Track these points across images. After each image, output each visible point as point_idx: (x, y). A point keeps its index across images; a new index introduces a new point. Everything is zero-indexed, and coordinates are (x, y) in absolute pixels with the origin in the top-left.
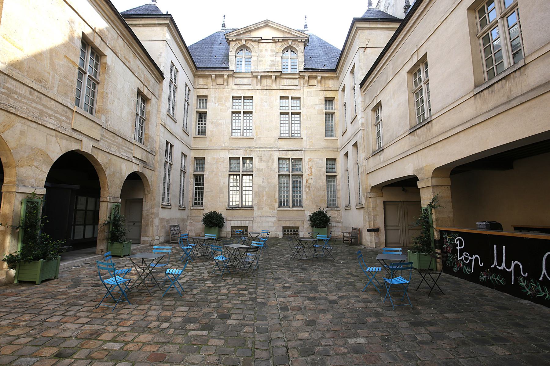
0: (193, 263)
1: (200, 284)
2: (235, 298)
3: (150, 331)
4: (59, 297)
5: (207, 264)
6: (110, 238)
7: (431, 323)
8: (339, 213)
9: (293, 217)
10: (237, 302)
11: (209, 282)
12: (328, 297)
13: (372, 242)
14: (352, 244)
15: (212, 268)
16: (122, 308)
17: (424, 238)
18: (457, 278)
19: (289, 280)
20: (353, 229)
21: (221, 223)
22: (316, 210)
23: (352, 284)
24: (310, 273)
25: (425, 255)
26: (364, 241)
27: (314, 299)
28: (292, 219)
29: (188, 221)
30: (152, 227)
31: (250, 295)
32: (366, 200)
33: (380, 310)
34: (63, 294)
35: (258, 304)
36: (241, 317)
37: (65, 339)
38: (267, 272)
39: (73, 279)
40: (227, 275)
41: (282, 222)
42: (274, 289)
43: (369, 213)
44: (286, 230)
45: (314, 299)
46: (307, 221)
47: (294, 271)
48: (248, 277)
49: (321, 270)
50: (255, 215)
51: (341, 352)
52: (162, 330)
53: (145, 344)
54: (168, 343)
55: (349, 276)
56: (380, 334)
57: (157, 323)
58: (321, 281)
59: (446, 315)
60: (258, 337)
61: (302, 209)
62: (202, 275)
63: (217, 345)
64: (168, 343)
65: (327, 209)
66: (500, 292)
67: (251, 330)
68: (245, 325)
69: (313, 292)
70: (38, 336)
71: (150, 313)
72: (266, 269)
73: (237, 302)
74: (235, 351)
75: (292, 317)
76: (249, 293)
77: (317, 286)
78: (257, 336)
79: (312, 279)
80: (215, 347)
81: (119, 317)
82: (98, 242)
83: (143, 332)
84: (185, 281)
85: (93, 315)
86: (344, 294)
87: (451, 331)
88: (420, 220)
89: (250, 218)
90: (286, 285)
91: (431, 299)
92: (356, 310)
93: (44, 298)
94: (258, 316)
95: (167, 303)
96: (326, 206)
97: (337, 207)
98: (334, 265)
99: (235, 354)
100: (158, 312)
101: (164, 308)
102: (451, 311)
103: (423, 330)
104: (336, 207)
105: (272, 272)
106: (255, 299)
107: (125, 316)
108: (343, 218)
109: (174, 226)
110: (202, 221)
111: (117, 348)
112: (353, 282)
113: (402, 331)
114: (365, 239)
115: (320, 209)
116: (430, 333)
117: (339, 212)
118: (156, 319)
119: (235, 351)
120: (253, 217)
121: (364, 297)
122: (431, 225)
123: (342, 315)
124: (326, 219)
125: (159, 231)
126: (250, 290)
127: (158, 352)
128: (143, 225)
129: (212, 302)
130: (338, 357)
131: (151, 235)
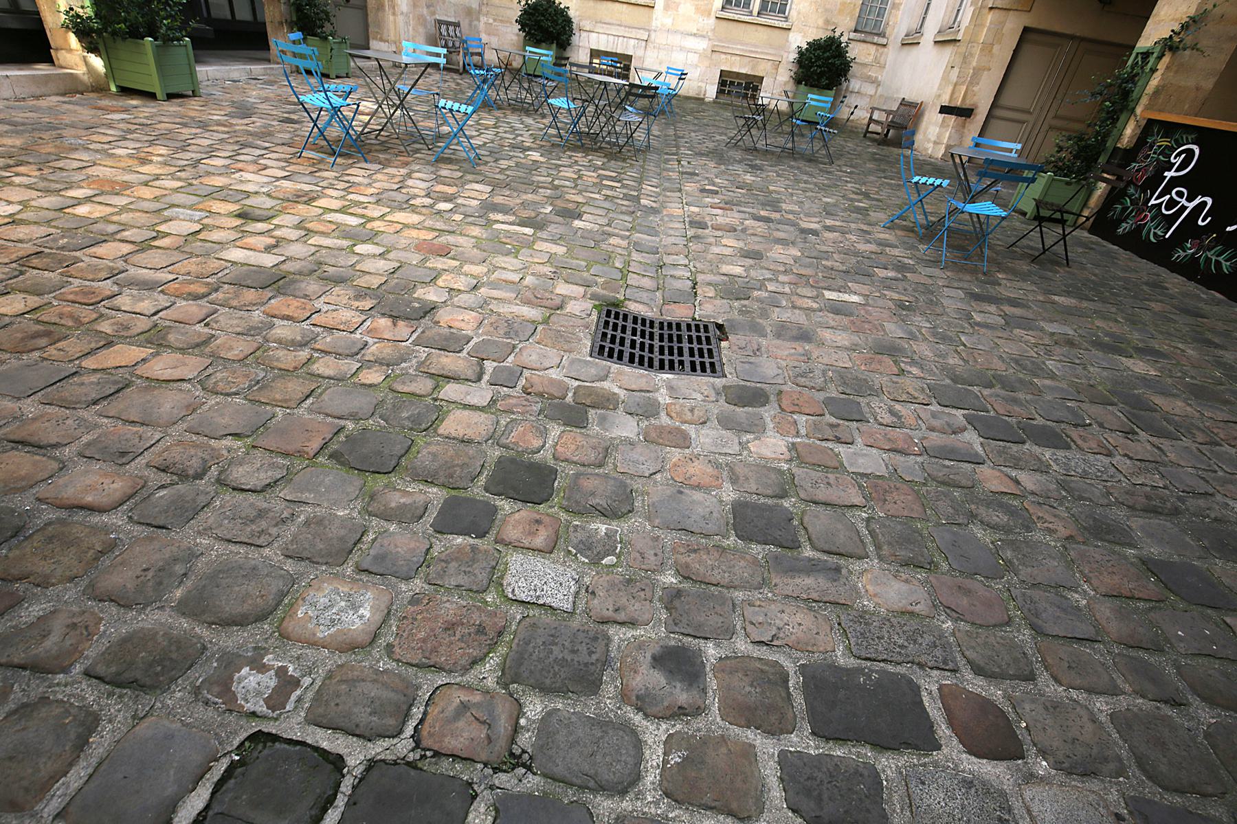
0: (498, 113)
1: (516, 154)
2: (591, 189)
3: (414, 209)
4: (215, 128)
5: (529, 121)
6: (296, 24)
7: (1014, 303)
8: (881, 54)
9: (756, 46)
10: (597, 196)
11: (534, 153)
12: (800, 222)
13: (938, 143)
14: (884, 141)
15: (541, 129)
16: (351, 166)
17: (1089, 139)
18: (1116, 247)
19: (718, 180)
20: (904, 103)
21: (565, 34)
22: (822, 35)
23: (863, 212)
24: (768, 176)
25: (1068, 183)
26: (919, 138)
27: (767, 220)
28: (752, 52)
29: (481, 18)
30: (394, 14)
31: (625, 191)
32: (977, 17)
33: (911, 262)
34: (219, 124)
35: (641, 208)
36: (604, 221)
37: (248, 194)
38: (669, 160)
39: (232, 101)
40: (575, 148)
41: (723, 56)
42: (680, 190)
43: (965, 59)
44: (727, 82)
45: (767, 220)
46: (788, 62)
47: (731, 168)
48: (624, 160)
49: (795, 175)
50: (655, 24)
51: (806, 306)
52: (439, 212)
53: (406, 226)
54: (453, 232)
55: (860, 197)
56: (896, 296)
57: (428, 201)
58: (792, 195)
59: (1056, 298)
60: (635, 256)
61: (784, 25)
62: (519, 138)
63: (553, 252)
64: (453, 232)
65: (852, 35)
66: (1204, 289)
67: (624, 243)
68: (610, 235)
69: (768, 208)
70: (195, 182)
71: (410, 182)
72: (667, 154)
73: (597, 196)
74: (588, 268)
75: (713, 240)
76: (623, 186)
77: (778, 201)
78: (633, 254)
79: (771, 188)
80: (549, 255)
81: (346, 178)
82: (269, 29)
83: (402, 209)
84: (481, 143)
85: (291, 168)
86: (838, 223)
87: (1052, 321)
88: (1111, 85)
89: (641, 31)
90: (707, 187)
91: (1035, 267)
92: (857, 253)
93: (185, 125)
94: (639, 225)
95: (444, 173)
96: (852, 25)
97: (882, 35)
98: (830, 172)
99: (588, 271)
100: (430, 184)
101: (439, 179)
102: (1068, 294)
103: (993, 308)
104: (878, 35)
105: (679, 162)
106: (638, 198)
107: (360, 179)
108: (885, 70)
109: (448, 24)
110: (516, 21)
111: (354, 224)
112: (866, 209)
113: (945, 302)
114: (925, 134)
115: (833, 31)
116: (1005, 316)
117: (881, 50)
118: (423, 193)
119: (588, 268)
120: (649, 31)
121: (882, 236)
122: (1132, 105)
123: (827, 255)
124: (841, 64)
125: (411, 28)
126: (625, 182)
127: (435, 241)
128: (369, 6)
129: (541, 187)
130: (797, 311)
131: (392, 37)
